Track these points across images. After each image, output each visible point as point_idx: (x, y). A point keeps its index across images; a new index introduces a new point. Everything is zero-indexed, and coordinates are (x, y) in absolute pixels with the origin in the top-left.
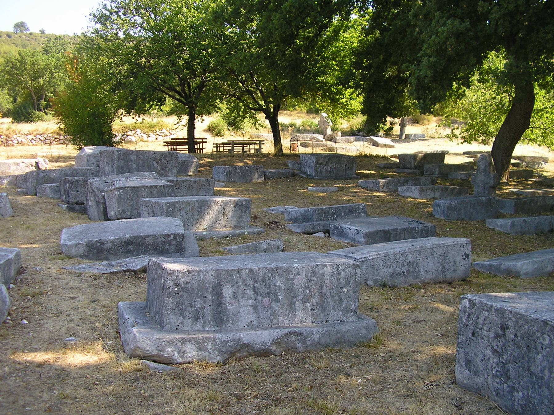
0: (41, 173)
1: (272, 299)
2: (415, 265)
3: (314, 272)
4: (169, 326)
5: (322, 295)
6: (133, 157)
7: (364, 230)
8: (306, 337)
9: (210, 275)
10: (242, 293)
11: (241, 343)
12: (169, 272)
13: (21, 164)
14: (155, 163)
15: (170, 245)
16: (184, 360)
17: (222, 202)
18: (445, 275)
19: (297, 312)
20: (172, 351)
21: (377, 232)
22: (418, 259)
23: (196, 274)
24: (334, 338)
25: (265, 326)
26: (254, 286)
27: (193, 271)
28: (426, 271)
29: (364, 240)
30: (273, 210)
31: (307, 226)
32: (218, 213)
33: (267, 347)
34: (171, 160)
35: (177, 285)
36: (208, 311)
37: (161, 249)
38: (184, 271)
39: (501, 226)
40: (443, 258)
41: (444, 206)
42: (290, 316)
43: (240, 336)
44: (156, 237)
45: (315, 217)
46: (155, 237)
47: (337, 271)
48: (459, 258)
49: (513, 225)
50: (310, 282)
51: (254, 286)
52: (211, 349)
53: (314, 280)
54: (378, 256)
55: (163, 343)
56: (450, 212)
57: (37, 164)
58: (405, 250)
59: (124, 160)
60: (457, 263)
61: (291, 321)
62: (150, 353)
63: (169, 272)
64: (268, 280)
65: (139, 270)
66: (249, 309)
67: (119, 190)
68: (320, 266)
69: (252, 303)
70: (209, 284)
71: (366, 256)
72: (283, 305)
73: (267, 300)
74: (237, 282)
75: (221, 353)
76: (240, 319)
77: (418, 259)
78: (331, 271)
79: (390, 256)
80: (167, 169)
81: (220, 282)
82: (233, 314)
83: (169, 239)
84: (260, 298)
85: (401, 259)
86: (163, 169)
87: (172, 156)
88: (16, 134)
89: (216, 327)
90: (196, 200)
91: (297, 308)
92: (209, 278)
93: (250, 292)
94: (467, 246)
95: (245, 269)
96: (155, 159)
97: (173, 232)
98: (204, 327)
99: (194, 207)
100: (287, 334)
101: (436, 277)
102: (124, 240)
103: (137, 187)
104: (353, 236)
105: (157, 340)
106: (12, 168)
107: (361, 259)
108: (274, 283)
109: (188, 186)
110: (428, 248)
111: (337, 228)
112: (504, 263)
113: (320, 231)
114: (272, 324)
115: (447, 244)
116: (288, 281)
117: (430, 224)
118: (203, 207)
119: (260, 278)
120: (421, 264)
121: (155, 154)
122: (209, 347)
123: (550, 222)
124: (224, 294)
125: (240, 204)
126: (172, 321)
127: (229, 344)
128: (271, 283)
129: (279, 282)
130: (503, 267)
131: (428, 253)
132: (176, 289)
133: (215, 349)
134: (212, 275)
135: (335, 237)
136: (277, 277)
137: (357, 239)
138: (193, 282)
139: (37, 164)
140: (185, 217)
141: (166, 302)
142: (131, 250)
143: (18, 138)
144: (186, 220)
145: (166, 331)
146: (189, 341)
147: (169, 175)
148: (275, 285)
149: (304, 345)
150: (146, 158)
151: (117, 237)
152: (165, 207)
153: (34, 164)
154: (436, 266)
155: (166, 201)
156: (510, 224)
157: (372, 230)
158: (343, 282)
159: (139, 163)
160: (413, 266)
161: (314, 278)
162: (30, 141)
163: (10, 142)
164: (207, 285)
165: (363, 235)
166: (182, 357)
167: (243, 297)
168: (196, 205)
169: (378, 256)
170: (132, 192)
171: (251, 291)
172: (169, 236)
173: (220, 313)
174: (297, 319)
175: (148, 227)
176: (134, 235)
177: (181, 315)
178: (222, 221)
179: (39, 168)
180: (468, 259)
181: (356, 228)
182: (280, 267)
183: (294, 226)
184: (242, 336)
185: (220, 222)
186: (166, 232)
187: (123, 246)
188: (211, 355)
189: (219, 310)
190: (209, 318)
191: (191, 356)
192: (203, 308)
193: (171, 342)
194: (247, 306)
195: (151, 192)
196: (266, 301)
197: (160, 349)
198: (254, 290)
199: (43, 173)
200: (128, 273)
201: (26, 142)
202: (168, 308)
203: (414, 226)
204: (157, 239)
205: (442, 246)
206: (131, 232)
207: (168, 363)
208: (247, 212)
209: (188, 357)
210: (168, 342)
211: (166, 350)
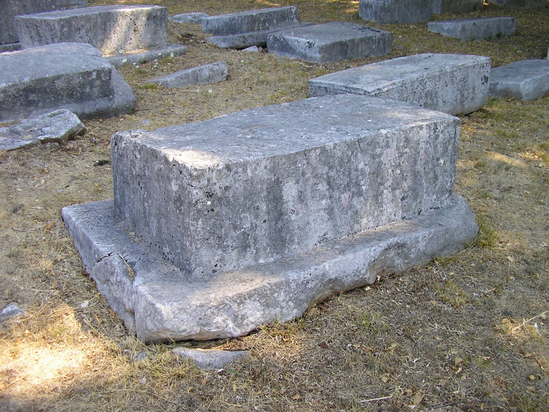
1: (353, 193)
2: (434, 95)
3: (407, 140)
4: (201, 269)
5: (415, 175)
7: (319, 43)
8: (409, 249)
9: (263, 166)
10: (312, 191)
11: (327, 279)
12: (195, 173)
15: (92, 87)
16: (244, 331)
17: (132, 13)
18: (463, 105)
19: (385, 207)
20: (224, 321)
21: (334, 45)
22: (437, 87)
23: (240, 170)
24: (442, 241)
25: (344, 237)
26: (328, 176)
27: (236, 165)
28: (445, 102)
29: (320, 56)
30: (179, 19)
31: (236, 39)
32: (127, 30)
33: (361, 276)
35: (209, 195)
36: (262, 231)
37: (78, 94)
38: (220, 167)
39: (448, 31)
40: (463, 84)
41: (376, 7)
42: (376, 214)
43: (325, 269)
44: (71, 78)
45: (245, 27)
46: (69, 78)
47: (434, 134)
48: (478, 82)
49: (463, 29)
50: (401, 156)
51: (328, 176)
52: (284, 301)
53: (406, 153)
54: (394, 86)
55: (209, 312)
56: (383, 14)
58: (423, 76)
60: (476, 89)
61: (377, 222)
62: (188, 333)
63: (195, 173)
64: (347, 163)
65: (63, 137)
66: (322, 216)
68: (415, 129)
69: (326, 204)
70: (262, 184)
71: (379, 87)
72: (366, 200)
73: (347, 196)
74: (304, 174)
75: (298, 303)
76: (309, 234)
77: (437, 87)
78: (428, 135)
79: (407, 86)
81: (278, 178)
82: (299, 227)
83: (90, 79)
84: (336, 194)
85: (419, 89)
89: (275, 254)
90: (97, 13)
91: (385, 200)
92: (262, 173)
93: (323, 187)
94: (487, 67)
95: (315, 149)
97: (96, 68)
98: (256, 260)
99: (96, 23)
100: (386, 249)
101: (454, 109)
102: (22, 87)
104: (303, 51)
105: (199, 308)
107: (374, 91)
108: (355, 165)
110: (447, 72)
111: (277, 40)
112: (500, 83)
113: (252, 44)
114: (353, 232)
115: (467, 66)
116: (374, 158)
117: (388, 32)
119: (337, 161)
120: (440, 94)
122: (281, 299)
123: (498, 25)
124: (285, 197)
125: (154, 14)
126: (205, 259)
127: (309, 286)
128: (352, 167)
129: (362, 163)
130: (499, 87)
131: (448, 79)
132: (209, 203)
133: (290, 300)
134: (266, 168)
135: (275, 52)
136: (359, 155)
137: (309, 55)
138: (237, 185)
141: (192, 228)
142: (34, 101)
145: (196, 280)
146: (250, 297)
148: (357, 170)
149: (406, 261)
151: (10, 84)
152: (57, 27)
154: (455, 94)
155: (58, 18)
156: (460, 28)
157: (328, 42)
158: (440, 149)
160: (431, 97)
161: (406, 149)
164: (259, 186)
165: (318, 49)
166: (239, 326)
167: (313, 197)
168: (99, 20)
169: (394, 86)
171: (325, 184)
172: (89, 74)
173: (280, 231)
174: (384, 218)
175: (53, 62)
176: (37, 78)
177: (220, 246)
178: (134, 41)
180: (487, 83)
181: (308, 41)
182: (364, 138)
183: (218, 40)
184: (327, 268)
185: (131, 41)
186: (84, 68)
187: (21, 95)
188: (285, 311)
189: (280, 227)
190: (264, 242)
191: (253, 321)
192: (254, 228)
193: (221, 307)
194: (319, 211)
196: (345, 196)
197: (204, 323)
198: (329, 183)
200: (48, 145)
202: (197, 238)
203: (371, 35)
204: (71, 80)
205: (462, 68)
206: (29, 73)
207: (216, 341)
208: (164, 25)
209: (249, 323)
210: (217, 307)
211: (214, 321)
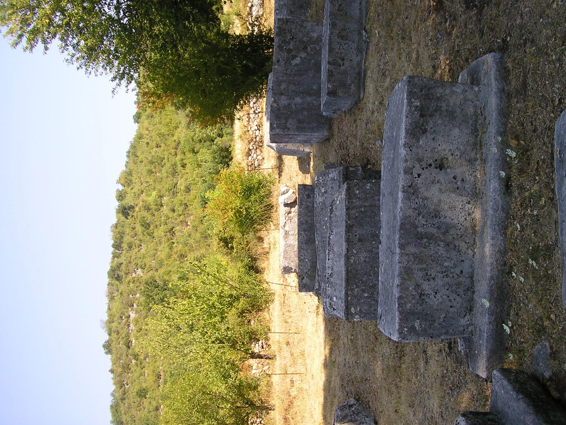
0: (304, 281)
6: (284, 101)
13: (287, 228)
14: (294, 62)
34: (290, 31)
57: (286, 205)
59: (287, 119)
67: (352, 314)
86: (305, 48)
87: (284, 30)
88: (248, 131)
103: (348, 272)
106: (292, 242)
118: (420, 229)
139: (286, 205)
140: (441, 283)
143: (253, 129)
144: (446, 279)
147: (315, 35)
150: (285, 78)
153: (287, 209)
159: (293, 91)
162: (257, 116)
163: (258, 139)
168: (412, 249)
170: (357, 287)
179: (295, 202)
195: (360, 240)
199: (303, 278)
201: (258, 120)
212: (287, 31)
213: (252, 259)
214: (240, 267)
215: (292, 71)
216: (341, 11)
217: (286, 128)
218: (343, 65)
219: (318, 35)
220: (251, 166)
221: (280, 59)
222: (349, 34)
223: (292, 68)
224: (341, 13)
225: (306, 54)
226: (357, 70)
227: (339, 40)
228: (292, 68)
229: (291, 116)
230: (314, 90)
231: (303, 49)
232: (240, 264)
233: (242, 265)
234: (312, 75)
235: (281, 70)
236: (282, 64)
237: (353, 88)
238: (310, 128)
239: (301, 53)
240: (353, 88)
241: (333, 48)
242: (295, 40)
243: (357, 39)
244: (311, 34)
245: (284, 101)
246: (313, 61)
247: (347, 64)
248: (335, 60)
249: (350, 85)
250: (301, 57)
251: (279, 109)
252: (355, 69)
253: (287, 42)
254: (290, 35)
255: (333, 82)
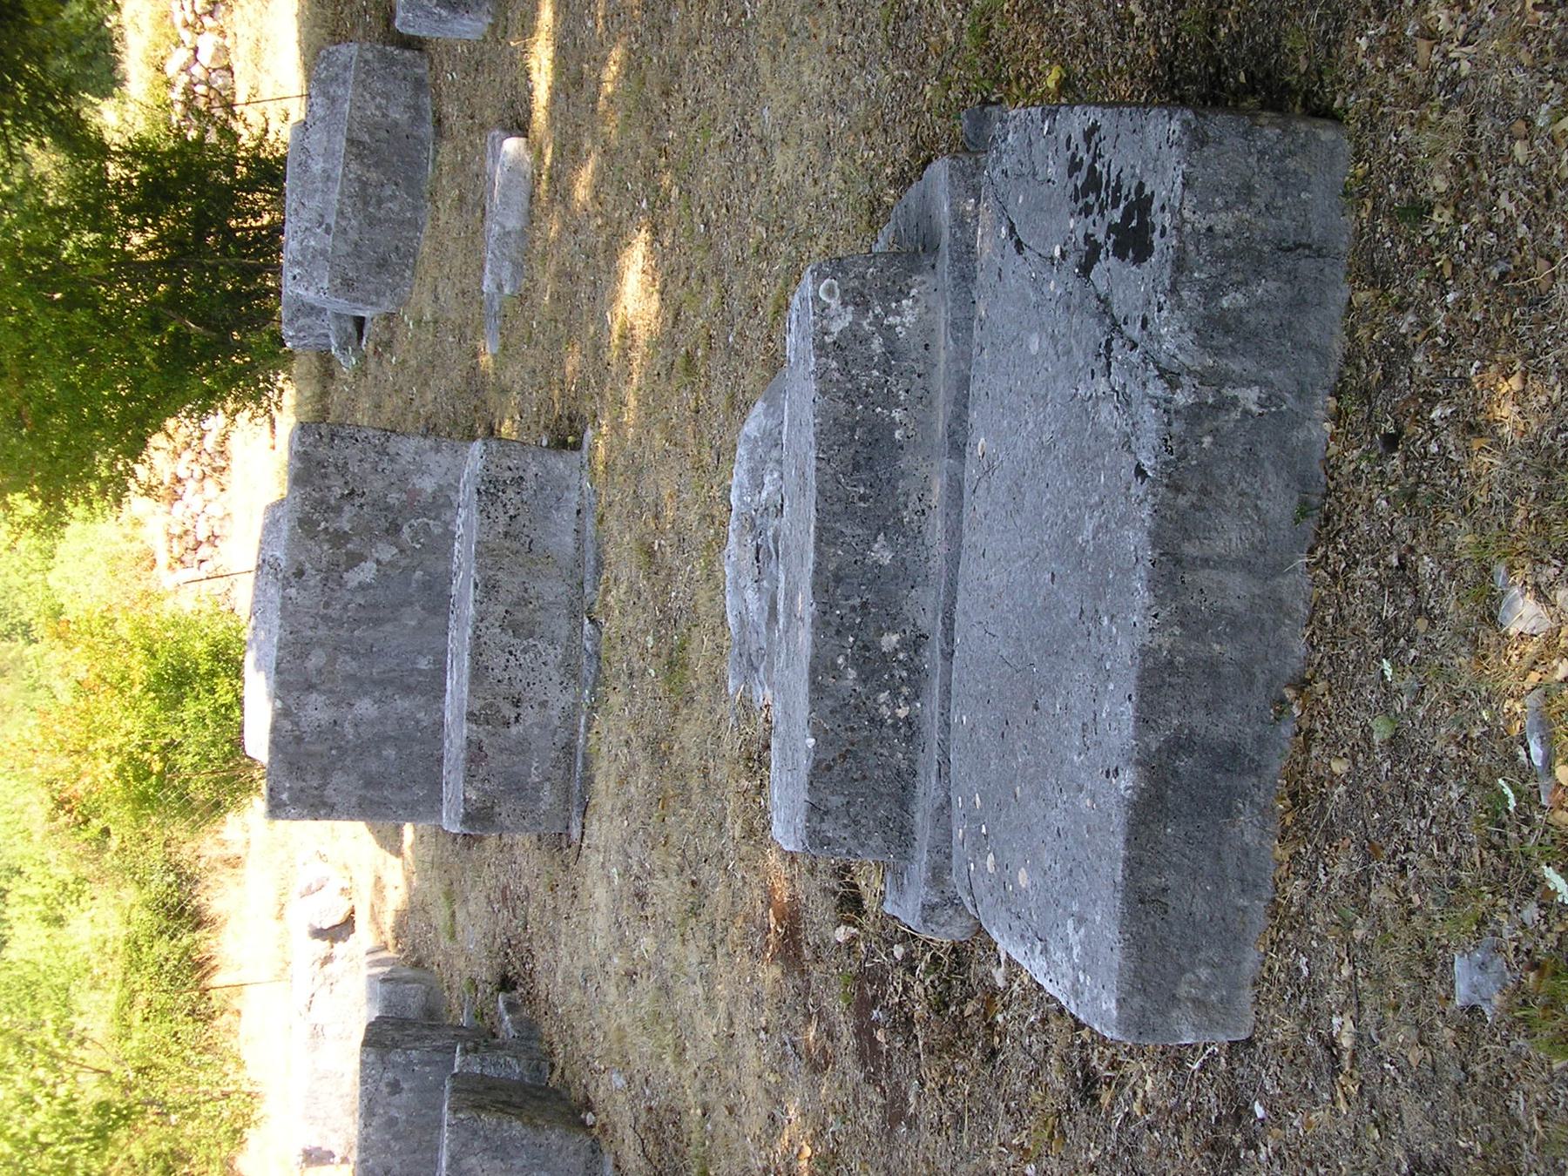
6: (317, 710)
14: (354, 577)
34: (342, 469)
59: (325, 773)
80: (394, 498)
86: (394, 529)
87: (321, 464)
96: (332, 574)
109: (507, 638)
121: (300, 573)
147: (427, 485)
150: (322, 631)
153: (322, 946)
212: (331, 469)
213: (178, 875)
214: (133, 906)
215: (345, 608)
216: (516, 537)
217: (324, 804)
218: (517, 719)
219: (439, 486)
220: (180, 537)
221: (308, 566)
222: (539, 616)
223: (348, 596)
224: (516, 545)
225: (395, 551)
226: (561, 737)
227: (505, 639)
228: (348, 596)
229: (339, 765)
230: (420, 672)
231: (387, 530)
232: (130, 894)
233: (141, 899)
234: (413, 623)
235: (308, 603)
236: (312, 583)
237: (548, 795)
238: (405, 805)
239: (380, 545)
240: (548, 795)
241: (487, 668)
242: (358, 501)
243: (564, 633)
244: (415, 480)
245: (317, 710)
246: (419, 574)
247: (530, 715)
248: (491, 705)
249: (537, 788)
250: (378, 562)
251: (299, 740)
252: (555, 734)
253: (330, 508)
254: (341, 482)
255: (483, 780)
